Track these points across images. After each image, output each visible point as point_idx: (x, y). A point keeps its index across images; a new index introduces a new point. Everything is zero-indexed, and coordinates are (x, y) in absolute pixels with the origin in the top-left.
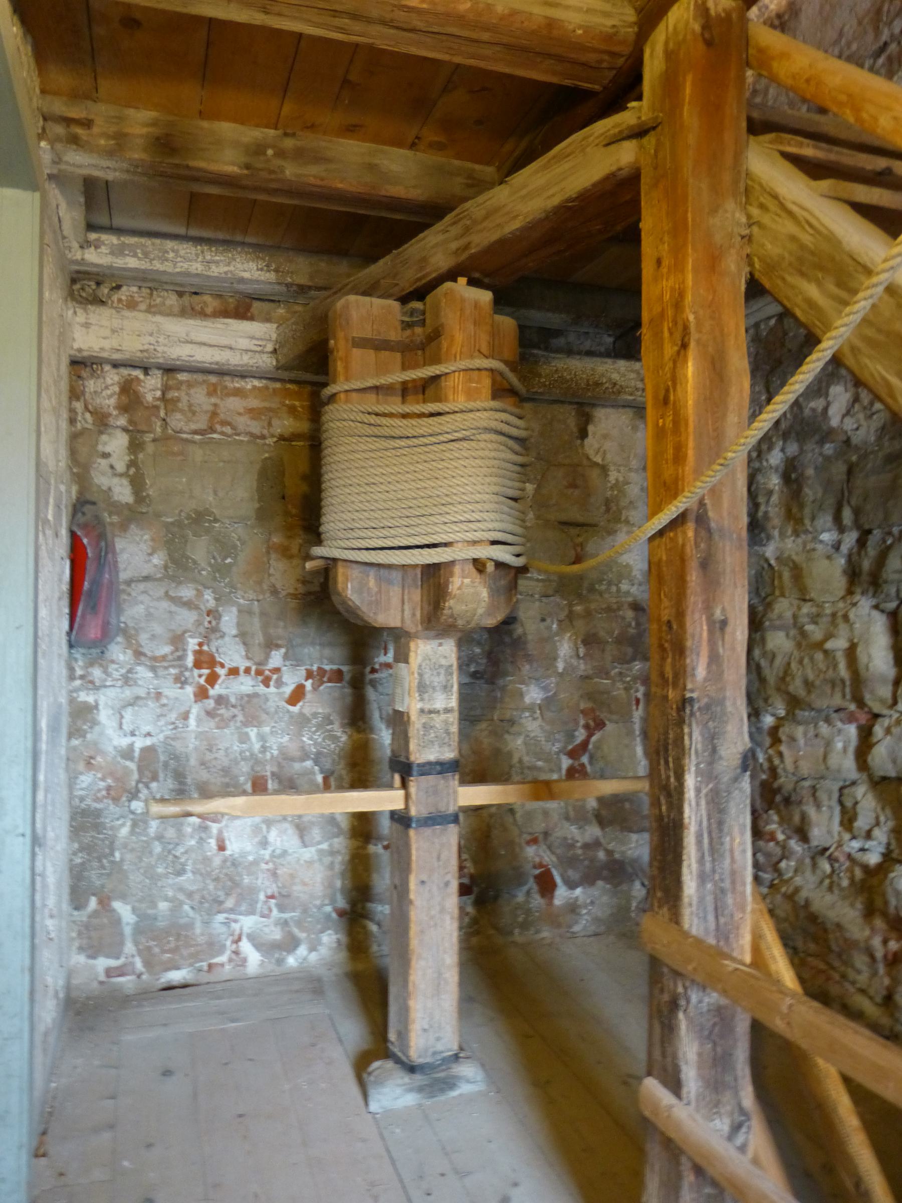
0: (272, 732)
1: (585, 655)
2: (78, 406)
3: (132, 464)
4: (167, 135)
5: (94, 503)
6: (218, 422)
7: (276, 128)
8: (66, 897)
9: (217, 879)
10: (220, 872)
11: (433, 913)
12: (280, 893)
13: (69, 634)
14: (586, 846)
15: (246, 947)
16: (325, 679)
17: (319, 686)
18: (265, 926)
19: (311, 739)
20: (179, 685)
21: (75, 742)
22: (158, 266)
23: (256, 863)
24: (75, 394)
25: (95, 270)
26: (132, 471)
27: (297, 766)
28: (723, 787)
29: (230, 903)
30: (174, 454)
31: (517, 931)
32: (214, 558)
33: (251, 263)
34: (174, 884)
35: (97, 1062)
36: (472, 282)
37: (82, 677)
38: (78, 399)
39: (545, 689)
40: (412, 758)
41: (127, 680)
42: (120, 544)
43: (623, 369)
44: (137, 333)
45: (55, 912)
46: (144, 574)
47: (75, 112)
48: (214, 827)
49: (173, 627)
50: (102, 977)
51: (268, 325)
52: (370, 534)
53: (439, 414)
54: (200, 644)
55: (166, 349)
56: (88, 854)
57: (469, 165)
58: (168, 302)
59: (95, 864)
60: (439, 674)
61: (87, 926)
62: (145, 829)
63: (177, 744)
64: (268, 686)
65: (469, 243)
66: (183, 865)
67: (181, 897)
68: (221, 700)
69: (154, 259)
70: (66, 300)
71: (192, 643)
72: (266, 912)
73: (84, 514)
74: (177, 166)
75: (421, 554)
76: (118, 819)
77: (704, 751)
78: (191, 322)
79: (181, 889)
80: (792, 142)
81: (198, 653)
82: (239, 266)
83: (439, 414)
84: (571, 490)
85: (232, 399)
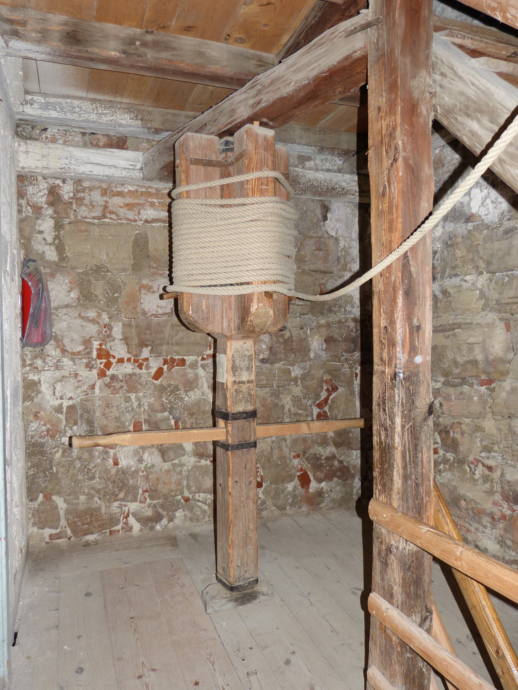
0: (144, 396)
1: (326, 348)
2: (23, 202)
3: (56, 237)
4: (74, 31)
5: (34, 261)
6: (108, 212)
7: (141, 29)
8: (25, 494)
9: (114, 482)
10: (115, 478)
11: (242, 499)
12: (150, 489)
13: (21, 339)
14: (327, 458)
15: (132, 520)
16: (175, 364)
17: (172, 368)
18: (142, 508)
19: (167, 399)
20: (89, 369)
21: (27, 404)
22: (69, 116)
23: (136, 471)
24: (21, 194)
25: (31, 118)
26: (57, 242)
27: (159, 415)
28: (417, 424)
29: (122, 495)
30: (81, 231)
31: (288, 508)
32: (107, 293)
33: (126, 115)
34: (89, 485)
35: (46, 589)
36: (262, 124)
37: (30, 365)
38: (23, 198)
39: (303, 368)
40: (229, 410)
41: (57, 367)
42: (51, 285)
43: (348, 180)
44: (58, 157)
45: (18, 503)
46: (66, 303)
47: (16, 16)
48: (112, 452)
49: (84, 335)
50: (47, 540)
51: (137, 153)
52: (202, 277)
53: (244, 205)
54: (101, 345)
55: (75, 167)
56: (38, 469)
57: (259, 53)
58: (76, 139)
59: (41, 475)
60: (244, 360)
61: (38, 511)
62: (70, 454)
63: (88, 404)
64: (141, 369)
65: (261, 100)
66: (94, 474)
67: (93, 492)
68: (113, 377)
69: (66, 112)
70: (13, 137)
71: (96, 344)
72: (143, 500)
73: (28, 267)
74: (80, 51)
75: (234, 289)
76: (54, 448)
77: (407, 403)
78: (91, 151)
79: (93, 488)
80: (459, 36)
81: (99, 350)
82: (118, 116)
83: (244, 205)
84: (318, 252)
85: (116, 198)
